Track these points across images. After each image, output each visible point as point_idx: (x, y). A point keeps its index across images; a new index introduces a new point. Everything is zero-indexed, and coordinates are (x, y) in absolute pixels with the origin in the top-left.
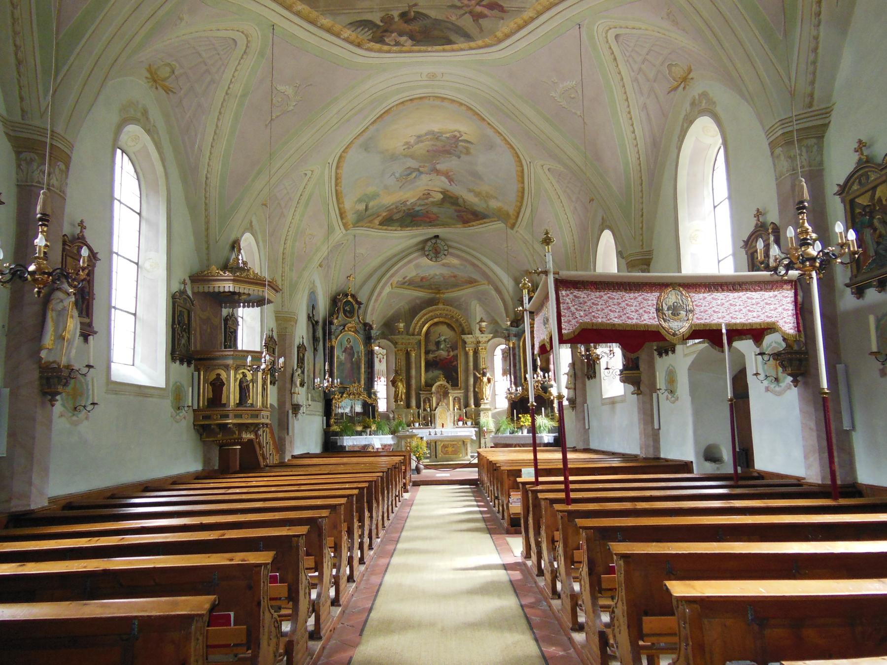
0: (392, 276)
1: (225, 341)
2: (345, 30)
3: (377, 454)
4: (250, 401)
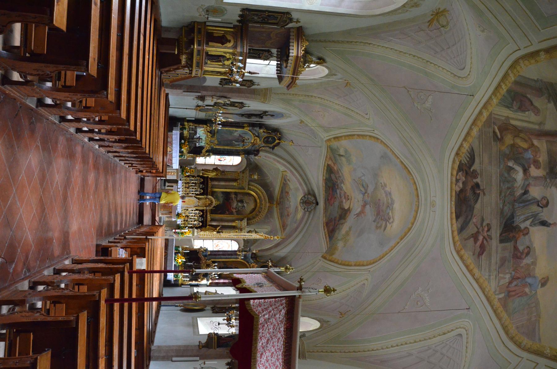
0: (291, 171)
1: (253, 50)
2: (468, 145)
3: (165, 153)
4: (209, 62)
